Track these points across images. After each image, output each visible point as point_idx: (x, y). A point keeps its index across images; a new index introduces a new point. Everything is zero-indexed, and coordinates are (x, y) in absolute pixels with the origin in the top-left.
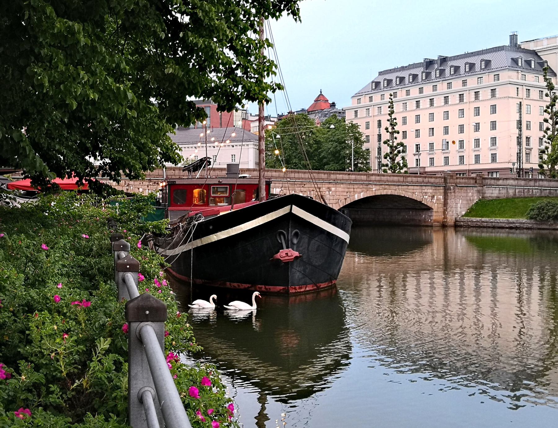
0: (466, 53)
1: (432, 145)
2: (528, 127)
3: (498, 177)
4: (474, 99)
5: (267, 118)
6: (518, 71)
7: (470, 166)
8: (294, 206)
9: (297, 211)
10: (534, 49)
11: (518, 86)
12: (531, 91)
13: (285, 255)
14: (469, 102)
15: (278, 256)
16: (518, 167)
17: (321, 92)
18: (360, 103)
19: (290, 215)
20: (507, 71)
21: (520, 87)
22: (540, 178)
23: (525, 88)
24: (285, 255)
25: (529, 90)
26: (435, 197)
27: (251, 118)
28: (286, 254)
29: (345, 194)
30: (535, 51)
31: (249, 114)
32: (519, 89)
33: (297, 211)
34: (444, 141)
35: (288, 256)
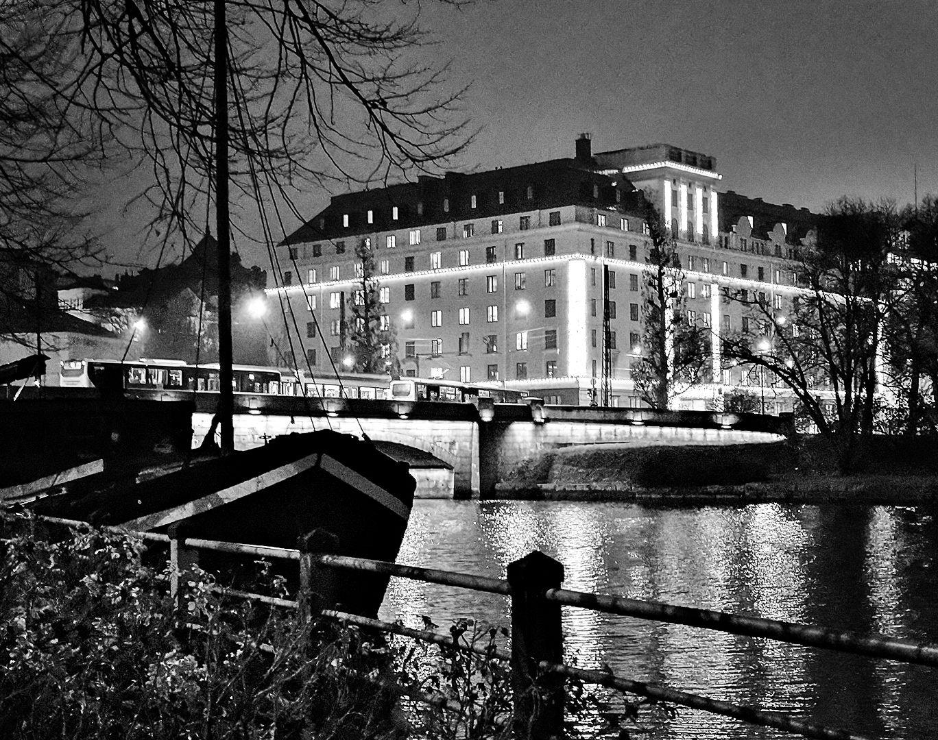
9: (332, 466)
26: (457, 444)
33: (332, 466)
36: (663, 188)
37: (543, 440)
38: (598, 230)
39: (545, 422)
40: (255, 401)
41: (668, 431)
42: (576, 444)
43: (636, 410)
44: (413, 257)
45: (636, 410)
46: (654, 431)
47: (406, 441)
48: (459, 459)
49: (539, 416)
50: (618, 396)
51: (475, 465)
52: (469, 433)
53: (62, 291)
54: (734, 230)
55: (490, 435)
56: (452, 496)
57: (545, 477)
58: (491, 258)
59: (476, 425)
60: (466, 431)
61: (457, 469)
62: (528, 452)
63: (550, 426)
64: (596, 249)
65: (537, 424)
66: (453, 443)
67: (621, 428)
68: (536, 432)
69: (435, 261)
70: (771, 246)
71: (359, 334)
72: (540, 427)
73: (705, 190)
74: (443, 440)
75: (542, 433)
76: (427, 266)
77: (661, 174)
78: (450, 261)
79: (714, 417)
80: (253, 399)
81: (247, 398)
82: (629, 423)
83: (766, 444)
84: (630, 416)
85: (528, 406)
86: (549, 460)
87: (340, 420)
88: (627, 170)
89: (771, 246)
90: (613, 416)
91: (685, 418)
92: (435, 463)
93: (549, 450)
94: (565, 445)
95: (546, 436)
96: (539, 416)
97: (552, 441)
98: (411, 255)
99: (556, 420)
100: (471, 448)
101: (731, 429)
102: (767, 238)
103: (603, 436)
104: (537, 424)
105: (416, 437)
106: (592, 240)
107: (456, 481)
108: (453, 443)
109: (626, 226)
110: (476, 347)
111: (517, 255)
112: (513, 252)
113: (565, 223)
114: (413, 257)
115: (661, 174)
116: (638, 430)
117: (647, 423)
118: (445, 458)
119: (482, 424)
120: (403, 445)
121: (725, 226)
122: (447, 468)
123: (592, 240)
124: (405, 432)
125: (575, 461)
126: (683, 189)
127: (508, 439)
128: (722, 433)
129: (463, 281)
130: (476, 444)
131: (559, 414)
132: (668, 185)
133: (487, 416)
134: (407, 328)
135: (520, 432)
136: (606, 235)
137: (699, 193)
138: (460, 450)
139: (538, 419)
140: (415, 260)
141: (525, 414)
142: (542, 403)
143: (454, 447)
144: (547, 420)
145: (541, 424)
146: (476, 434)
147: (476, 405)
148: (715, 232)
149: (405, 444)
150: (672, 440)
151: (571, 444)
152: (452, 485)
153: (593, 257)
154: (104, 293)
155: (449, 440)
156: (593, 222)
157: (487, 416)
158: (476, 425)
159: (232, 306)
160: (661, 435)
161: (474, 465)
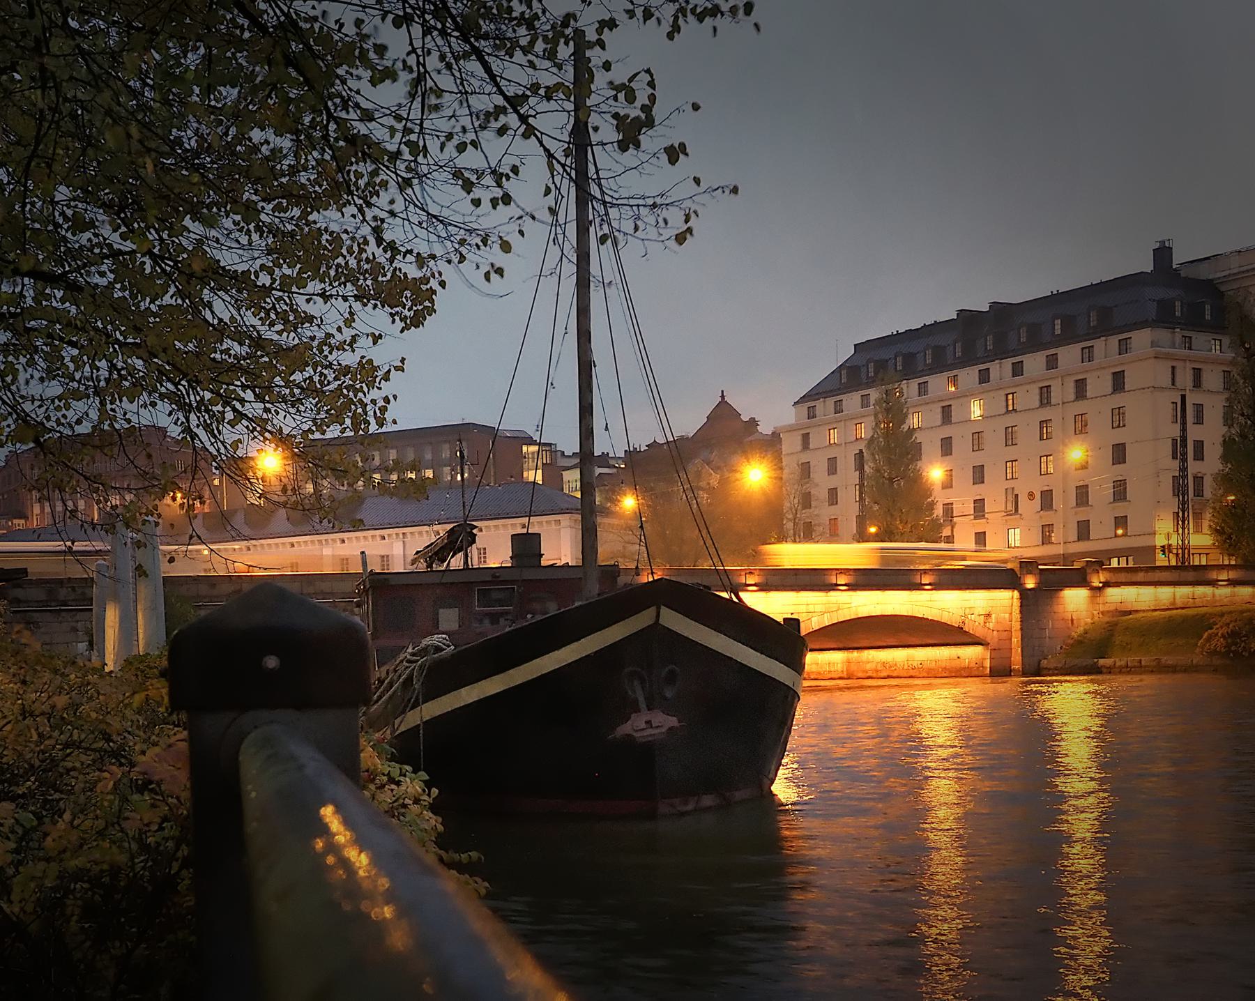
0: (1055, 292)
2: (1199, 456)
3: (1131, 565)
4: (1072, 397)
5: (604, 459)
6: (1174, 328)
7: (1068, 545)
8: (664, 610)
9: (673, 620)
10: (1211, 277)
11: (1174, 364)
12: (1193, 339)
13: (643, 725)
14: (1063, 403)
15: (625, 729)
16: (1180, 543)
17: (723, 397)
18: (814, 416)
19: (656, 627)
20: (1176, 431)
21: (1178, 364)
22: (1226, 562)
23: (1189, 366)
24: (643, 725)
25: (1200, 369)
26: (993, 616)
27: (563, 462)
28: (646, 722)
30: (1211, 280)
31: (559, 454)
32: (1178, 372)
33: (673, 620)
34: (1009, 492)
35: (651, 727)
37: (1102, 608)
39: (1103, 586)
40: (752, 576)
42: (1144, 611)
43: (1222, 567)
44: (1124, 371)
45: (1222, 567)
47: (919, 612)
48: (995, 632)
50: (1207, 554)
51: (1016, 640)
52: (1007, 603)
53: (567, 472)
59: (1016, 594)
60: (1003, 601)
61: (993, 643)
62: (1083, 624)
63: (1111, 592)
67: (1201, 590)
68: (1093, 599)
74: (976, 612)
75: (1100, 600)
80: (751, 573)
81: (743, 573)
82: (1213, 583)
83: (793, 590)
84: (1214, 575)
85: (1083, 568)
90: (1191, 576)
94: (1130, 612)
97: (1112, 608)
98: (1080, 377)
99: (1118, 584)
104: (1093, 589)
105: (943, 609)
108: (989, 615)
110: (1029, 508)
113: (955, 423)
114: (1124, 371)
116: (1223, 592)
117: (1232, 583)
118: (979, 632)
119: (1024, 594)
120: (928, 619)
122: (982, 645)
124: (929, 604)
127: (1059, 609)
131: (1122, 577)
133: (1030, 583)
134: (1076, 469)
135: (1074, 600)
139: (1096, 584)
140: (1088, 381)
142: (1101, 564)
143: (989, 620)
144: (1107, 584)
145: (1099, 589)
146: (1017, 603)
149: (930, 618)
152: (987, 664)
154: (614, 470)
157: (1030, 583)
158: (1016, 594)
159: (599, 520)
161: (1014, 640)
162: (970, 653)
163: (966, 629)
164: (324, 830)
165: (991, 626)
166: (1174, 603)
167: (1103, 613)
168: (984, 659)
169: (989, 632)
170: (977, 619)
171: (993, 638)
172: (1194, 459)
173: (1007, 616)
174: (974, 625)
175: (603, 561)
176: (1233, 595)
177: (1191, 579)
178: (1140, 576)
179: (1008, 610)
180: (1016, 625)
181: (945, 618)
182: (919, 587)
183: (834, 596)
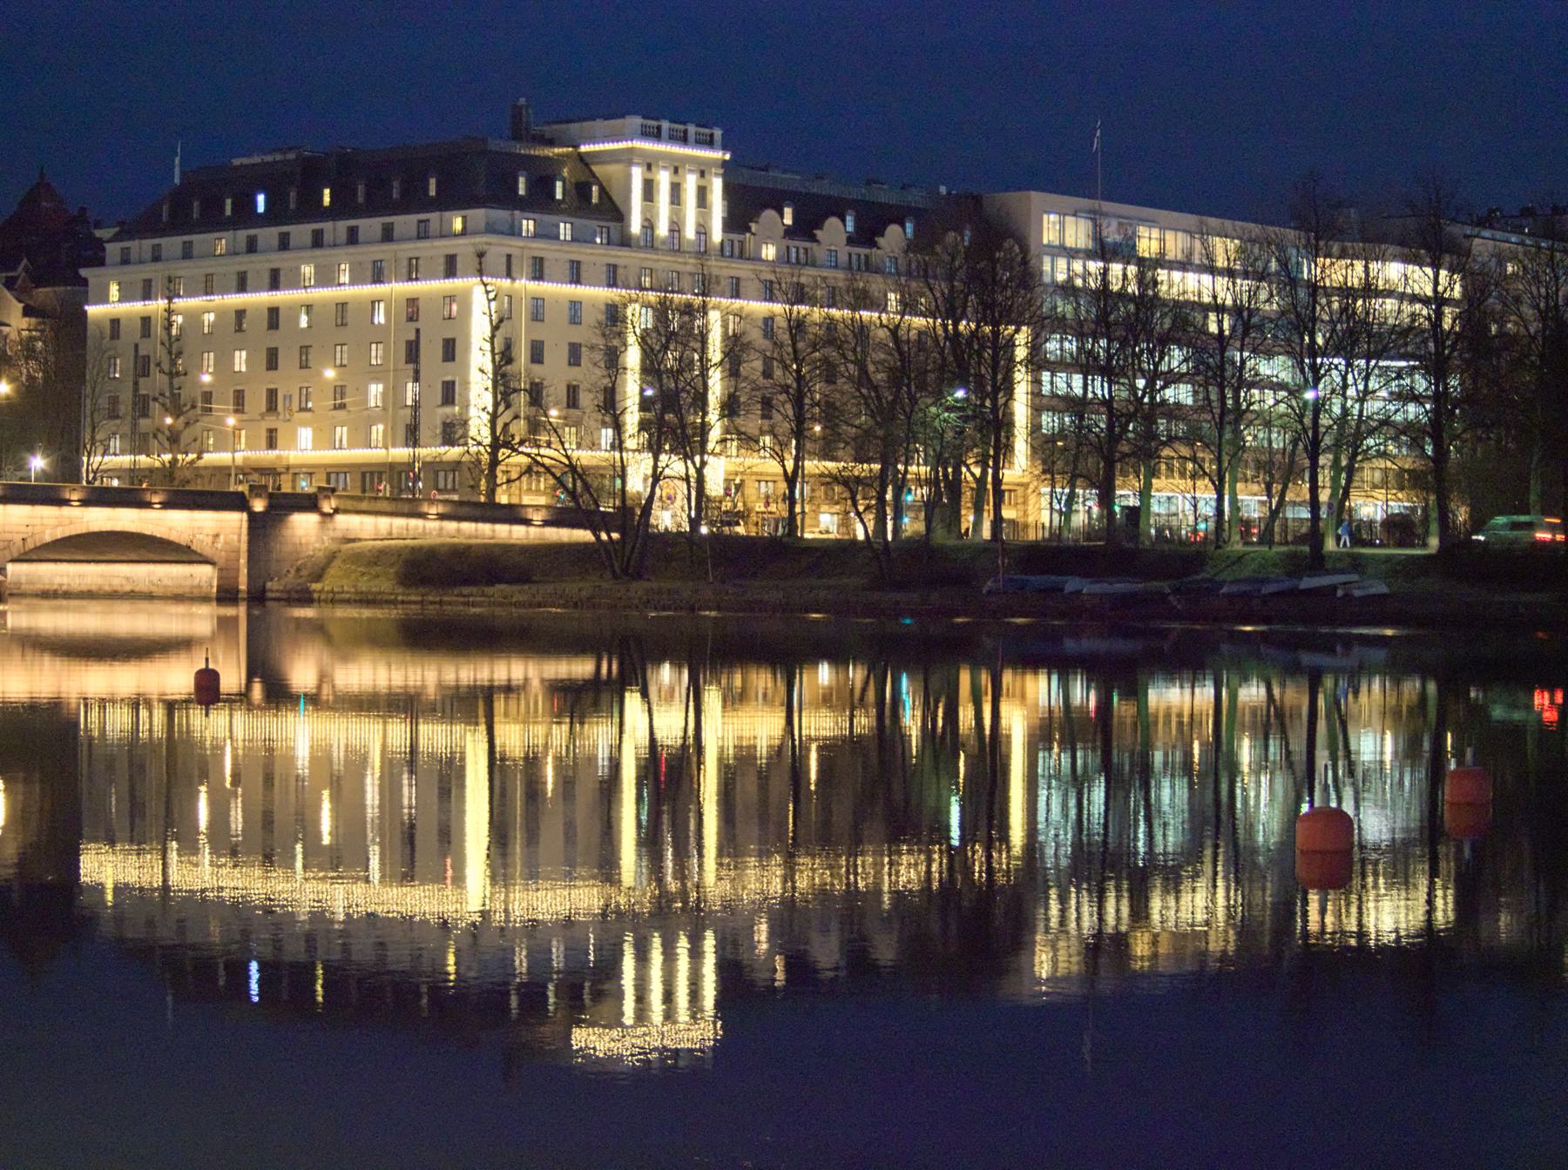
1: (272, 394)
26: (222, 537)
29: (24, 529)
36: (628, 178)
37: (331, 533)
38: (521, 243)
41: (468, 527)
46: (451, 526)
47: (148, 530)
49: (327, 507)
51: (243, 561)
52: (237, 524)
54: (753, 230)
55: (262, 529)
56: (214, 595)
57: (318, 576)
58: (378, 278)
59: (245, 516)
60: (232, 524)
61: (221, 563)
63: (340, 518)
64: (514, 268)
65: (324, 515)
66: (217, 536)
67: (414, 523)
68: (323, 523)
69: (307, 275)
70: (819, 252)
71: (162, 394)
72: (328, 519)
73: (702, 174)
74: (205, 532)
75: (330, 526)
76: (296, 283)
77: (628, 158)
78: (326, 278)
79: (523, 511)
82: (423, 516)
86: (332, 557)
87: (83, 509)
88: (584, 149)
89: (819, 252)
91: (1060, 464)
92: (195, 558)
93: (334, 547)
94: (354, 540)
95: (334, 529)
96: (327, 507)
99: (346, 512)
100: (239, 541)
101: (543, 526)
102: (814, 239)
103: (394, 531)
104: (324, 515)
105: (170, 529)
106: (509, 257)
107: (219, 578)
108: (217, 536)
109: (562, 231)
111: (410, 273)
112: (405, 270)
115: (628, 158)
116: (433, 525)
118: (208, 552)
119: (253, 518)
121: (737, 221)
123: (509, 257)
125: (356, 558)
126: (664, 178)
127: (287, 532)
128: (532, 530)
129: (342, 306)
130: (245, 538)
131: (349, 504)
132: (637, 174)
135: (303, 524)
136: (530, 248)
137: (691, 182)
138: (226, 543)
139: (327, 508)
141: (309, 504)
144: (337, 511)
145: (330, 515)
146: (245, 525)
147: (247, 493)
148: (717, 235)
150: (470, 537)
151: (360, 540)
153: (509, 281)
155: (212, 533)
156: (514, 231)
157: (259, 506)
158: (245, 516)
160: (458, 530)
162: (204, 575)
163: (194, 547)
164: (183, 173)
165: (219, 546)
166: (390, 533)
167: (333, 539)
168: (212, 578)
169: (218, 550)
170: (205, 539)
171: (221, 558)
172: (570, 364)
173: (235, 537)
174: (202, 544)
175: (645, 488)
176: (458, 530)
177: (406, 511)
178: (364, 505)
179: (237, 531)
180: (244, 547)
181: (173, 537)
182: (148, 505)
183: (66, 510)
